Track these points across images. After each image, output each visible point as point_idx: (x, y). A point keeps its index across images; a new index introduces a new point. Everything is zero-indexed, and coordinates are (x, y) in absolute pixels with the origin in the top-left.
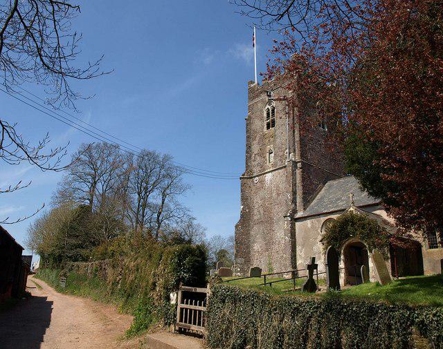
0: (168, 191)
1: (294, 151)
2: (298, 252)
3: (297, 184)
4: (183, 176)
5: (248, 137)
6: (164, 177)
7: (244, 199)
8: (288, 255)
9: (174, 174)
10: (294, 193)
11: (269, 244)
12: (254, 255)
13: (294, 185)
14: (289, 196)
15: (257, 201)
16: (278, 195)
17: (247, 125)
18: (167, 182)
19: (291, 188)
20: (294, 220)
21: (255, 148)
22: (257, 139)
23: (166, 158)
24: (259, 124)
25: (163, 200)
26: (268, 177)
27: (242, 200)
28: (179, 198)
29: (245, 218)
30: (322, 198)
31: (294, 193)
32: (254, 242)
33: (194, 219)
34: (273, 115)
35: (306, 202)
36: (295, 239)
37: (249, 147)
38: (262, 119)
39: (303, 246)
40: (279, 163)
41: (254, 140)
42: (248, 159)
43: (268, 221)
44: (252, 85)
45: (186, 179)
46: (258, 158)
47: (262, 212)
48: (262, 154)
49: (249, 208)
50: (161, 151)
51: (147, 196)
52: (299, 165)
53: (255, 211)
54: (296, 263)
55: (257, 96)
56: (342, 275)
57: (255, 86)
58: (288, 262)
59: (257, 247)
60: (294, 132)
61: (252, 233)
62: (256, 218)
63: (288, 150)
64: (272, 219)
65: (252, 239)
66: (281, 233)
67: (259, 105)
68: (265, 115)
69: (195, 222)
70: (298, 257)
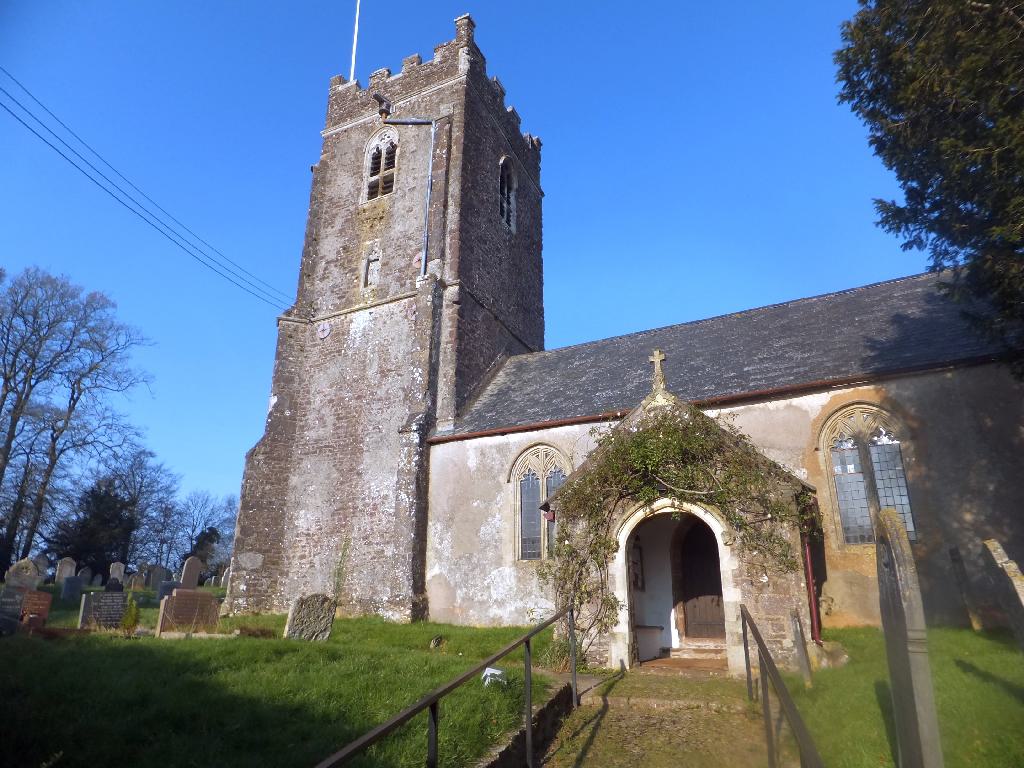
0: (87, 382)
1: (442, 255)
2: (432, 540)
3: (443, 346)
4: (134, 350)
5: (315, 215)
6: (83, 344)
7: (284, 381)
8: (399, 550)
9: (111, 345)
10: (433, 370)
11: (343, 511)
12: (293, 546)
13: (435, 345)
14: (419, 375)
15: (320, 387)
16: (384, 373)
17: (315, 182)
18: (87, 357)
19: (427, 352)
20: (427, 443)
21: (330, 246)
22: (339, 222)
23: (96, 302)
24: (348, 185)
25: (74, 400)
26: (360, 321)
27: (277, 380)
28: (114, 400)
29: (278, 443)
30: (503, 393)
31: (433, 370)
32: (298, 505)
33: (151, 454)
34: (390, 163)
35: (463, 398)
36: (427, 503)
37: (312, 240)
38: (357, 172)
39: (449, 522)
40: (394, 287)
41: (331, 224)
42: (307, 273)
43: (348, 447)
44: (341, 88)
45: (137, 359)
46: (335, 271)
47: (330, 420)
48: (347, 259)
49: (294, 406)
50: (85, 280)
51: (31, 387)
52: (452, 292)
53: (311, 417)
54: (423, 576)
55: (351, 115)
56: (9, 600)
57: (348, 89)
58: (403, 573)
59: (305, 520)
60: (445, 206)
61: (294, 480)
62: (310, 435)
63: (422, 255)
64: (358, 440)
65: (291, 497)
66: (383, 481)
67: (355, 136)
68: (368, 162)
69: (151, 462)
70: (430, 554)
